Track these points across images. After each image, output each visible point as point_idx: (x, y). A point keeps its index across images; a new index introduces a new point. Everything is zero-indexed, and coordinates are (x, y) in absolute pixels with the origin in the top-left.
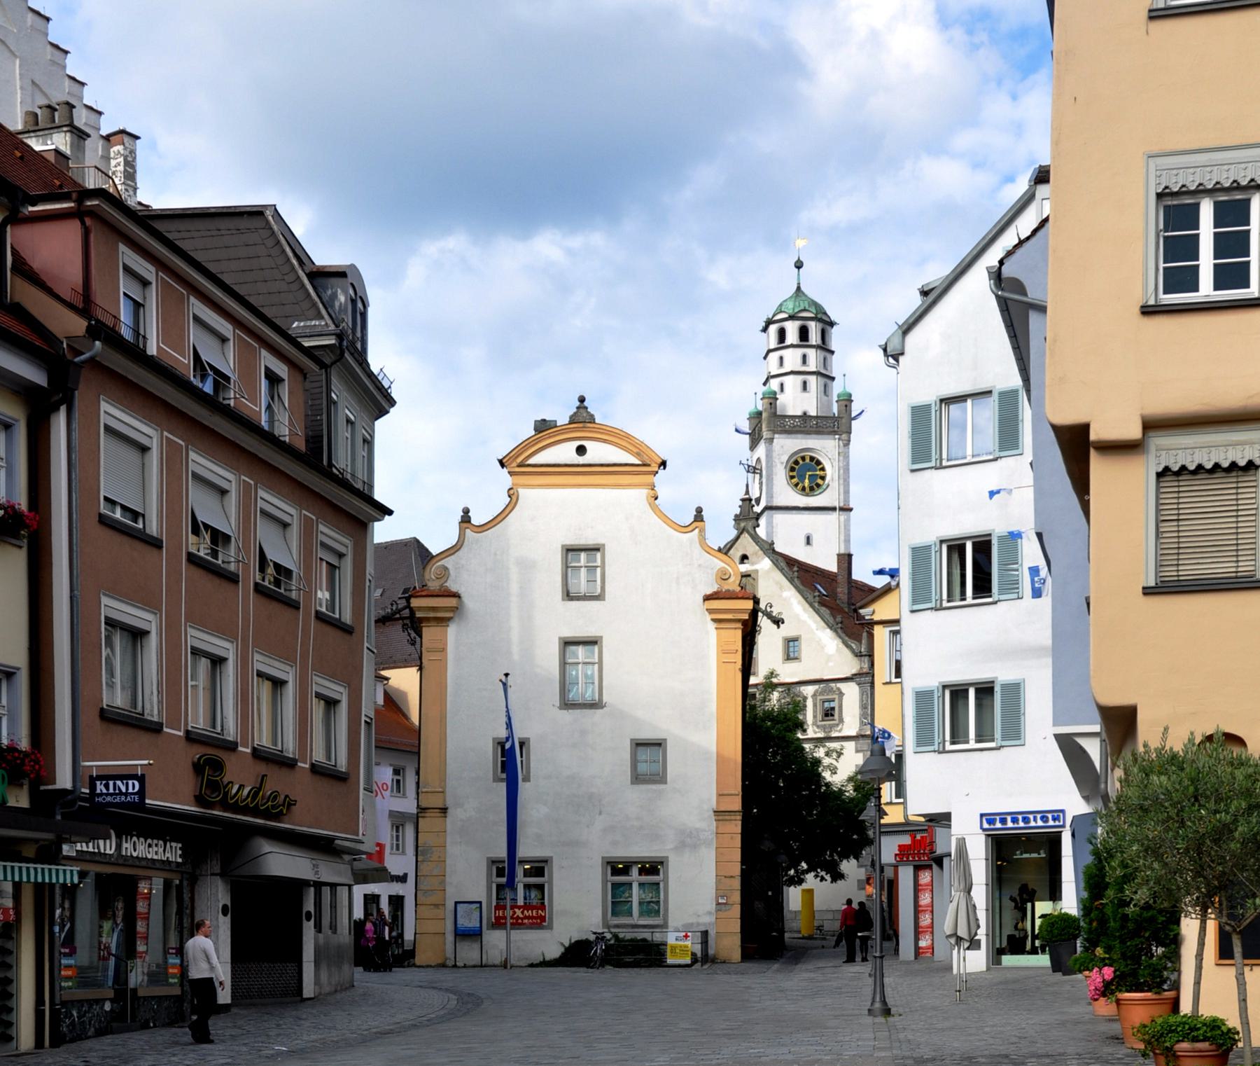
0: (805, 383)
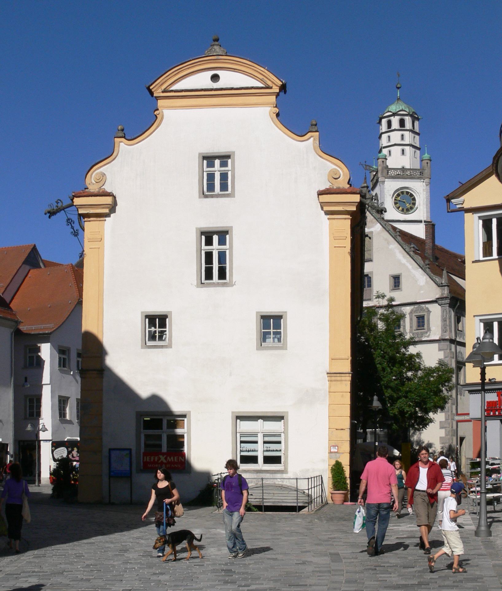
0: (403, 150)
